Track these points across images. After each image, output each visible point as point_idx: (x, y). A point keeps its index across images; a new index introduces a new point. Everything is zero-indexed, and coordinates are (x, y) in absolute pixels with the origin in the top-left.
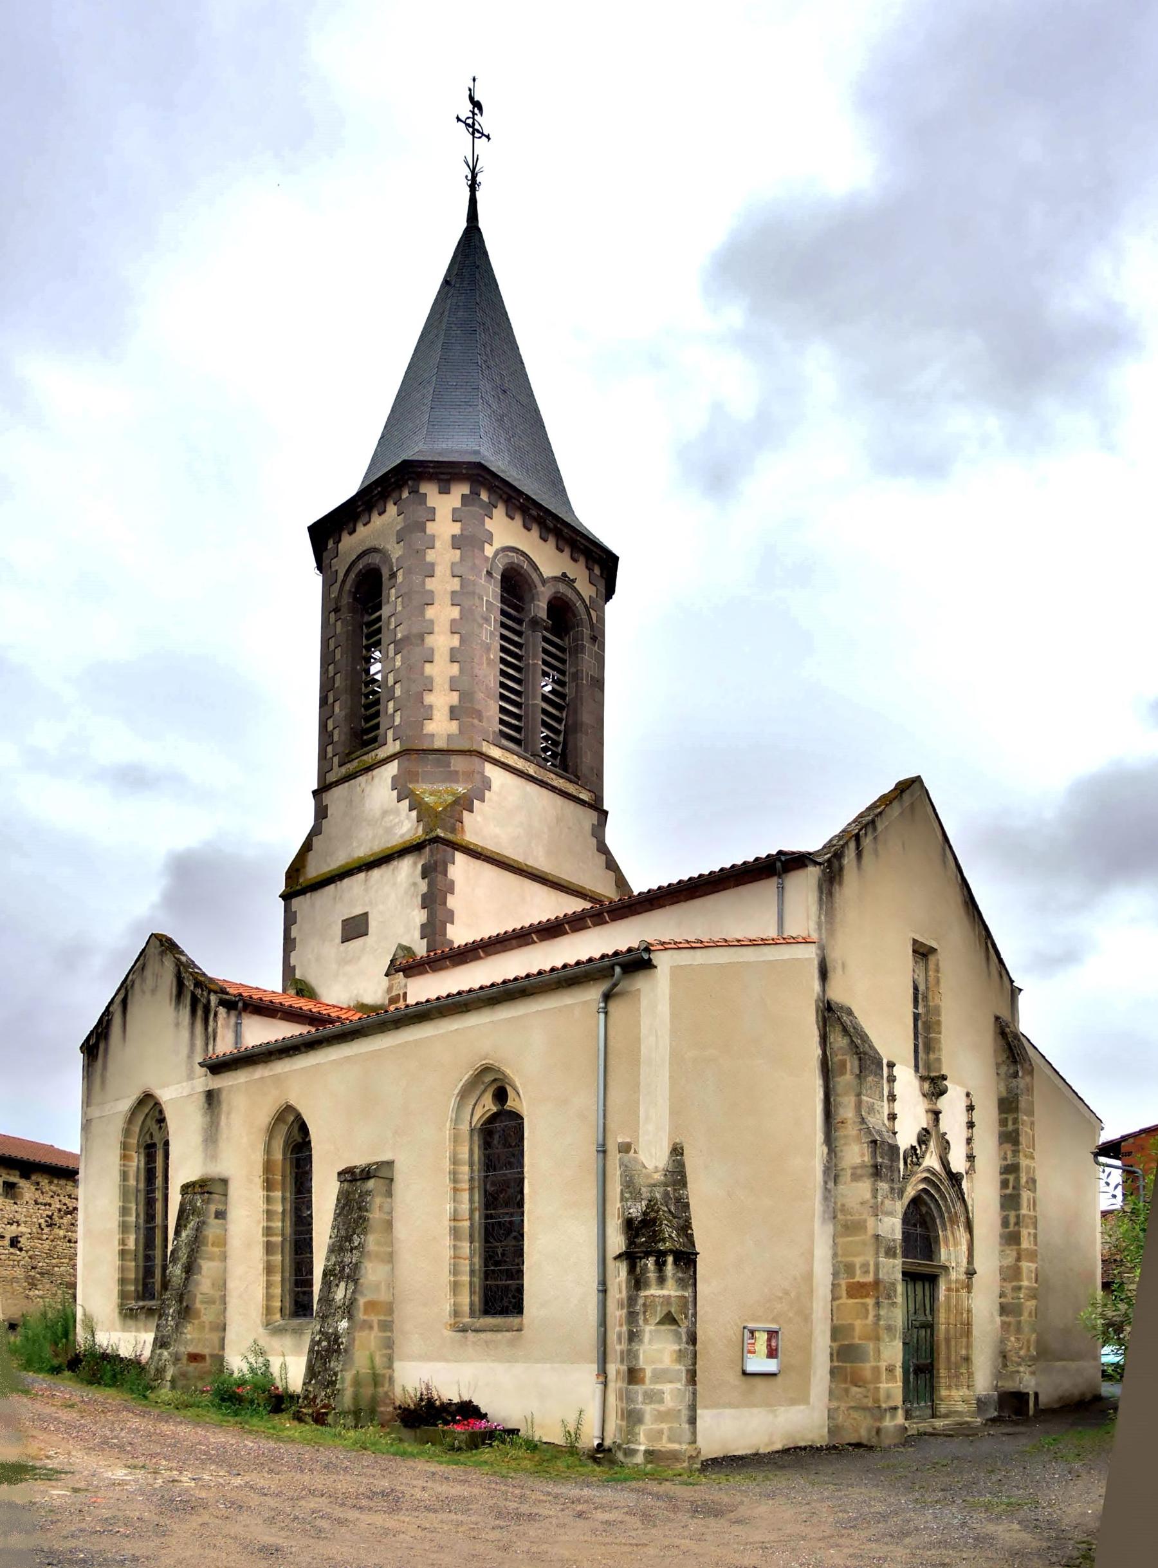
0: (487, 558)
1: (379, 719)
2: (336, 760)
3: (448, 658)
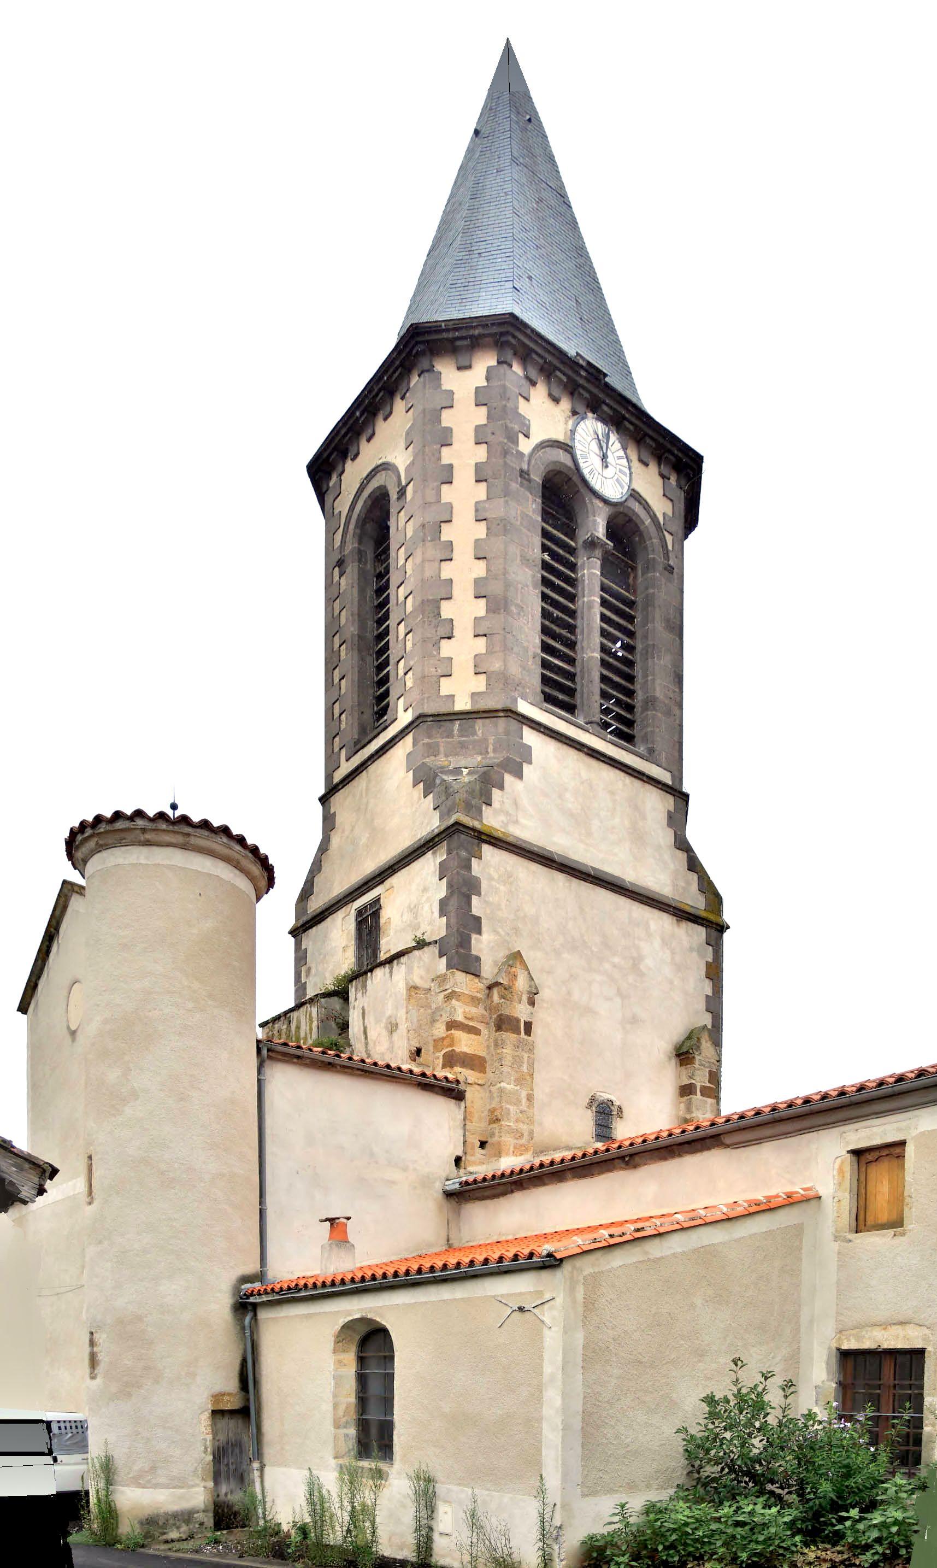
0: (522, 454)
1: (389, 591)
2: (343, 752)
3: (471, 670)
